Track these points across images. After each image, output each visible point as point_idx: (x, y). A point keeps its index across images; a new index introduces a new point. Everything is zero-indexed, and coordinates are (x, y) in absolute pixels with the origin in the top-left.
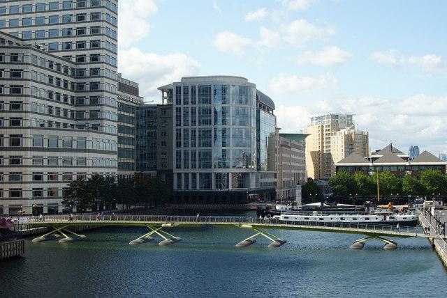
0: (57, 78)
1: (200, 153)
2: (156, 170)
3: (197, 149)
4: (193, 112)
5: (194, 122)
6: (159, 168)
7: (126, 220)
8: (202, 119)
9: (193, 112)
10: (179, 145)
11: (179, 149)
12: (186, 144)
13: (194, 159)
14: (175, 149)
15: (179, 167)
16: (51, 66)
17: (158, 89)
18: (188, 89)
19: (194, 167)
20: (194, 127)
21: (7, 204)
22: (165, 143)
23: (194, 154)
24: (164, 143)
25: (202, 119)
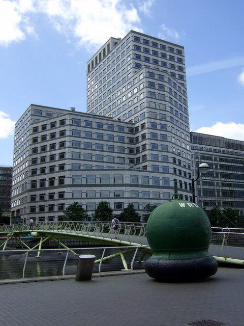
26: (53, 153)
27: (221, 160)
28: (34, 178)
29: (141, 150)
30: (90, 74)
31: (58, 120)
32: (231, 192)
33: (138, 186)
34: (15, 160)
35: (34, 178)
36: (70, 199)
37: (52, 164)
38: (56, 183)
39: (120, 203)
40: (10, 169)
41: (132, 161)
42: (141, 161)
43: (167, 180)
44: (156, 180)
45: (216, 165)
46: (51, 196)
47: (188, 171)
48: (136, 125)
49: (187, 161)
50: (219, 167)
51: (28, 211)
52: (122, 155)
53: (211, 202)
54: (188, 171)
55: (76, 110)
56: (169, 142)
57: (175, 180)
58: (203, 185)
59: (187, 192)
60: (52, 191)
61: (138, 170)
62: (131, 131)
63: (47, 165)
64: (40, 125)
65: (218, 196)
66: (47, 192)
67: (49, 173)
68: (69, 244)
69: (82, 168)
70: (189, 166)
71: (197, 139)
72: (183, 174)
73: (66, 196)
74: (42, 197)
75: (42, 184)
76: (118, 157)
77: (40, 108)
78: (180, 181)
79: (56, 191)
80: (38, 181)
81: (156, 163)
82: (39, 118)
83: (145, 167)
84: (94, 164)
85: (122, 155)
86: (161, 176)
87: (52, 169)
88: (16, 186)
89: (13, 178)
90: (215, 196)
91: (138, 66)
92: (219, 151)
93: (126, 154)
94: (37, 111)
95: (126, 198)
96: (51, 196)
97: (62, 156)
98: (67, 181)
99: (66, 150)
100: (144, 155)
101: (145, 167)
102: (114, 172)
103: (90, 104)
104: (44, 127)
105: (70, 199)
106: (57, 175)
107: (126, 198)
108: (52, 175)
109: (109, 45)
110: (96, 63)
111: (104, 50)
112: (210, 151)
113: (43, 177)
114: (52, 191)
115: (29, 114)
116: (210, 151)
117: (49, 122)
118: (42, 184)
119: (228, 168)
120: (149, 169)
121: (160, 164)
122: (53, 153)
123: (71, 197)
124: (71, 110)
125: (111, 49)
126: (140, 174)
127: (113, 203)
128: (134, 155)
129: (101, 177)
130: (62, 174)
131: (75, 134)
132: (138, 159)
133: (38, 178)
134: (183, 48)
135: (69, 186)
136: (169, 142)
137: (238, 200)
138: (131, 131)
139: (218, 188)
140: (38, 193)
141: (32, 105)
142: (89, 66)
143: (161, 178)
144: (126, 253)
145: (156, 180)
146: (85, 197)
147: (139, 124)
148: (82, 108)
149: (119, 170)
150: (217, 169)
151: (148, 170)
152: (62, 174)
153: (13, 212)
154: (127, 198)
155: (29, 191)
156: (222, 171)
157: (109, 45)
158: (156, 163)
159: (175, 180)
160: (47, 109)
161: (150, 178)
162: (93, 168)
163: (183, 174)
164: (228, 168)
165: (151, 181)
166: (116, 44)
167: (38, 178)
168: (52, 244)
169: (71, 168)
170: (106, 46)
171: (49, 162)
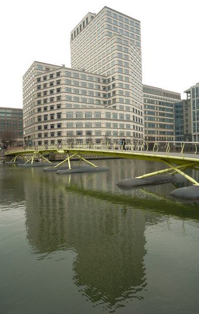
26: (52, 96)
30: (73, 41)
31: (55, 72)
32: (165, 125)
34: (24, 102)
37: (52, 104)
38: (56, 117)
40: (21, 110)
41: (105, 103)
44: (122, 116)
47: (140, 110)
48: (108, 78)
51: (37, 137)
52: (99, 99)
54: (140, 110)
55: (65, 67)
57: (134, 116)
59: (140, 124)
60: (46, 124)
61: (110, 109)
62: (104, 81)
63: (55, 104)
64: (42, 76)
66: (49, 124)
67: (57, 110)
69: (73, 107)
70: (141, 108)
71: (147, 89)
72: (135, 111)
77: (42, 64)
79: (56, 123)
80: (49, 115)
82: (40, 71)
83: (115, 107)
85: (99, 99)
86: (125, 113)
88: (26, 120)
89: (24, 115)
91: (109, 34)
94: (38, 65)
97: (59, 98)
98: (64, 116)
99: (61, 94)
102: (85, 110)
103: (73, 63)
104: (45, 78)
106: (55, 112)
108: (52, 112)
109: (87, 19)
110: (75, 36)
111: (84, 22)
113: (46, 113)
114: (46, 124)
115: (33, 69)
116: (153, 97)
117: (48, 74)
119: (163, 109)
120: (118, 108)
122: (52, 96)
124: (62, 66)
125: (89, 21)
126: (112, 112)
130: (59, 111)
131: (69, 83)
134: (139, 22)
135: (65, 119)
138: (104, 81)
139: (157, 122)
140: (43, 125)
141: (35, 62)
142: (72, 35)
145: (122, 116)
147: (110, 77)
148: (69, 66)
152: (59, 111)
153: (25, 138)
155: (37, 123)
157: (87, 19)
158: (122, 105)
159: (134, 116)
160: (45, 65)
163: (135, 111)
164: (163, 109)
165: (125, 117)
166: (92, 17)
170: (85, 19)
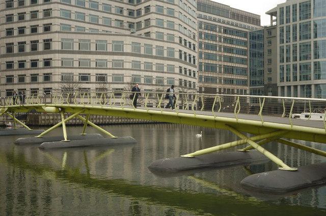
0: (190, 70)
1: (300, 67)
2: (264, 85)
3: (298, 62)
4: (295, 68)
5: (295, 39)
6: (266, 83)
7: (244, 110)
8: (302, 55)
9: (295, 28)
10: (282, 61)
11: (282, 45)
12: (288, 59)
13: (295, 51)
14: (279, 64)
15: (282, 80)
16: (181, 41)
17: (267, 13)
18: (290, 8)
19: (295, 79)
20: (295, 43)
21: (153, 3)
22: (271, 78)
23: (295, 28)
24: (270, 61)
25: (302, 55)
26: (35, 9)
27: (225, 31)
28: (10, 40)
29: (143, 12)
33: (140, 56)
35: (10, 40)
36: (58, 68)
38: (41, 47)
39: (103, 74)
41: (131, 25)
42: (143, 26)
43: (171, 51)
44: (160, 50)
45: (220, 37)
46: (34, 64)
47: (192, 42)
49: (193, 31)
50: (222, 40)
53: (212, 79)
56: (176, 5)
57: (180, 51)
58: (205, 59)
60: (22, 58)
61: (139, 36)
65: (220, 72)
66: (28, 59)
68: (98, 121)
69: (73, 30)
73: (54, 64)
74: (22, 65)
75: (22, 49)
76: (116, 20)
78: (185, 53)
79: (41, 58)
81: (161, 30)
83: (148, 34)
84: (87, 26)
86: (166, 45)
87: (21, 31)
90: (216, 72)
92: (224, 22)
93: (125, 16)
95: (126, 69)
96: (22, 65)
98: (56, 46)
100: (139, 22)
101: (148, 34)
105: (58, 68)
107: (126, 69)
112: (215, 20)
113: (22, 39)
114: (22, 58)
118: (22, 49)
119: (231, 41)
120: (153, 36)
121: (166, 31)
122: (35, 9)
123: (60, 65)
126: (143, 42)
127: (95, 74)
128: (134, 18)
129: (64, 42)
130: (47, 37)
132: (139, 23)
133: (16, 40)
136: (176, 5)
137: (239, 78)
140: (16, 60)
143: (154, 46)
144: (220, 140)
145: (160, 50)
146: (78, 66)
149: (117, 35)
150: (221, 42)
151: (151, 37)
152: (47, 37)
154: (128, 69)
156: (226, 45)
159: (180, 51)
161: (141, 45)
162: (86, 31)
164: (231, 41)
167: (16, 40)
168: (43, 122)
169: (59, 30)
171: (18, 22)
